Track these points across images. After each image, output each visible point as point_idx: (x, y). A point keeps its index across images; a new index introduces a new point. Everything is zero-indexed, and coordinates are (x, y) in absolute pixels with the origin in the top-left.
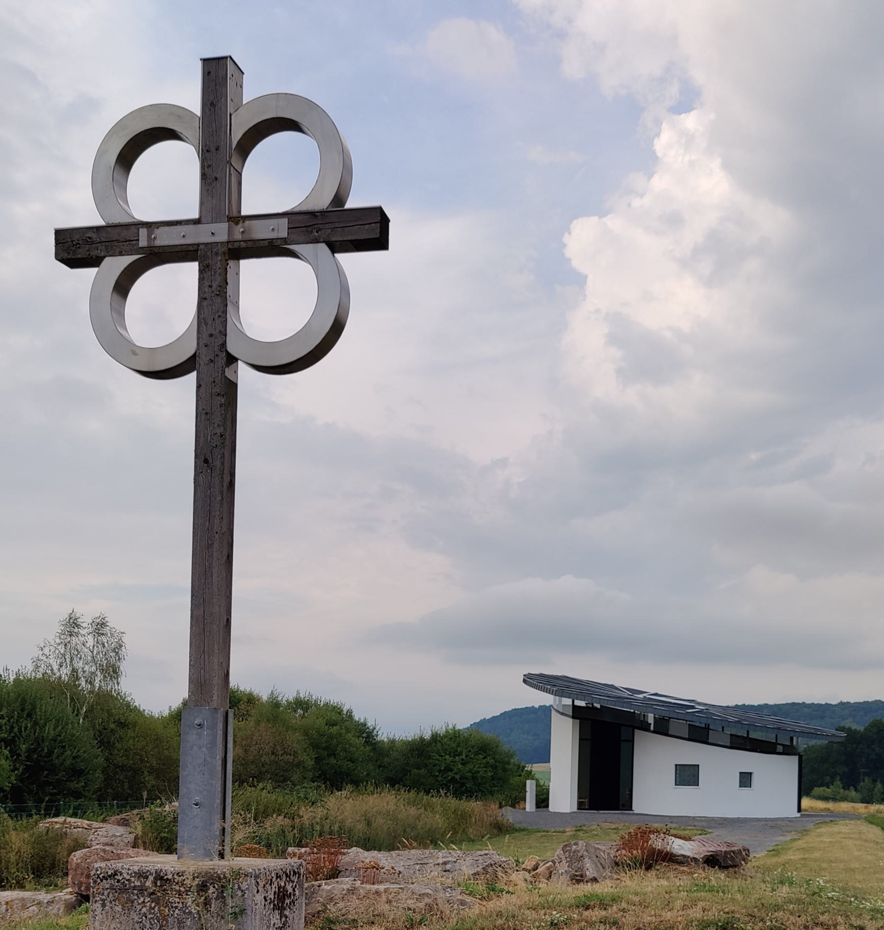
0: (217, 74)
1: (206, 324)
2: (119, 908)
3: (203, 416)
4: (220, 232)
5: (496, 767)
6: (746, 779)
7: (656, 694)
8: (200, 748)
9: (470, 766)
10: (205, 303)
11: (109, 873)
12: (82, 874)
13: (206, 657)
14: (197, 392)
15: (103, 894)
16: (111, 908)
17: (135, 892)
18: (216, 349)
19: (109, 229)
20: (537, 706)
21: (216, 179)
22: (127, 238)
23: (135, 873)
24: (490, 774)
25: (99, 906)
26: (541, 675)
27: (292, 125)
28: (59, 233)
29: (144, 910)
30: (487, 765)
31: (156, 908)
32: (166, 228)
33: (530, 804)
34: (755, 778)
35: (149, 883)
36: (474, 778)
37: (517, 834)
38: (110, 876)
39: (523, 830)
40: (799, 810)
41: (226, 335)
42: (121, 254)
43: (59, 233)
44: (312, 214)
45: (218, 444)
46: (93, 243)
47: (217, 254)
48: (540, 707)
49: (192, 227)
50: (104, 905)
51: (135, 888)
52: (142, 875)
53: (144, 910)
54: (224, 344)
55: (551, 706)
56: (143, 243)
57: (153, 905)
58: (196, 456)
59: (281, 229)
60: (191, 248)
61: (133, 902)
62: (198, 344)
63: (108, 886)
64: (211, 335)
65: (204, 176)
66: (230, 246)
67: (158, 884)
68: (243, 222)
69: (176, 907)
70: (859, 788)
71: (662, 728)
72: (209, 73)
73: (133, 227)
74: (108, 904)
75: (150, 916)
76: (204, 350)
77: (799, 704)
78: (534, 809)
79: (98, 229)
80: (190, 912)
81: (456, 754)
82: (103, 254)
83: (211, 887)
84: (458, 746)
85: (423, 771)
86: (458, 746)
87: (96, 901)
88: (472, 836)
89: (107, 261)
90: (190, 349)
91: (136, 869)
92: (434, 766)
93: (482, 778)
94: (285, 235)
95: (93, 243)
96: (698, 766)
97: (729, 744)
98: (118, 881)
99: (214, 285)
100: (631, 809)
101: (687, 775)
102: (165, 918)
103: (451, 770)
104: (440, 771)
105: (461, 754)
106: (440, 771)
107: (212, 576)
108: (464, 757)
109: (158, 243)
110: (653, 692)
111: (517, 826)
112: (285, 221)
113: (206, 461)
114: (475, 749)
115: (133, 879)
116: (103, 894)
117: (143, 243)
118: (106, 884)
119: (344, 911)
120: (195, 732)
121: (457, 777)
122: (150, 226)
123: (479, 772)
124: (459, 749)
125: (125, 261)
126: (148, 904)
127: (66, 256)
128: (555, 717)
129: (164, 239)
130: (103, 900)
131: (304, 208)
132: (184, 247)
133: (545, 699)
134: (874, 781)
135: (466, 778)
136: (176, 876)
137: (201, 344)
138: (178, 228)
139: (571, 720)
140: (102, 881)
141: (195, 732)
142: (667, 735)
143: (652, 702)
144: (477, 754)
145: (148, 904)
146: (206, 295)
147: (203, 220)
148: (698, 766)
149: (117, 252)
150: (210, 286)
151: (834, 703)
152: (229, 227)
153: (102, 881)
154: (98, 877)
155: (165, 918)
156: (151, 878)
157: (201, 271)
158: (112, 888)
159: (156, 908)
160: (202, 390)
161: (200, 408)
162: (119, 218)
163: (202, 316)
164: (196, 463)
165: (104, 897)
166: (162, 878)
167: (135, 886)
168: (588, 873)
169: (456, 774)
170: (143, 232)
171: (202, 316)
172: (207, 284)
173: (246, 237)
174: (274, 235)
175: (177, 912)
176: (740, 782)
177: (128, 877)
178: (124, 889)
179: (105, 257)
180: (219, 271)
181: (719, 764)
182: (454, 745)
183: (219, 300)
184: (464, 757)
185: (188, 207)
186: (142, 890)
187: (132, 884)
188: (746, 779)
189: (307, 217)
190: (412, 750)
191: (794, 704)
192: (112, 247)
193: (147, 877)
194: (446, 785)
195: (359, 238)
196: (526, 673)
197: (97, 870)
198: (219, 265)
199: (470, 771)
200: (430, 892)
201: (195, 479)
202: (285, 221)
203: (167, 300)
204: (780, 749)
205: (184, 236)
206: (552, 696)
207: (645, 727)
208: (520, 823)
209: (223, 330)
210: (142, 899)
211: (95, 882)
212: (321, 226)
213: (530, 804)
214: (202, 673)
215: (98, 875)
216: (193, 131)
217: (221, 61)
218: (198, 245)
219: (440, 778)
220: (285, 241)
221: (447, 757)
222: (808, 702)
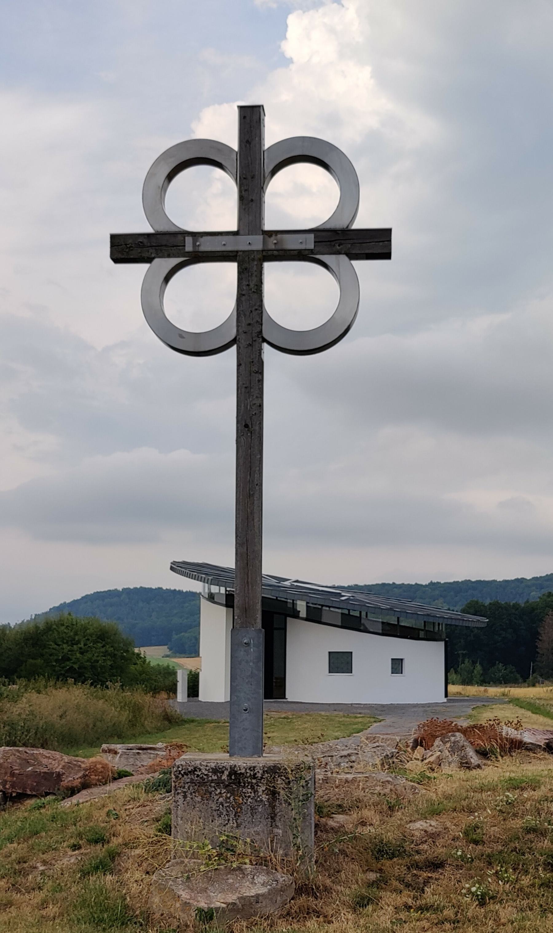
0: (251, 119)
1: (245, 315)
2: (199, 799)
3: (243, 390)
4: (256, 243)
5: (115, 655)
6: (397, 666)
7: (297, 581)
8: (247, 662)
9: (89, 655)
10: (243, 298)
11: (190, 770)
12: (6, 773)
13: (250, 587)
14: (238, 370)
15: (184, 788)
16: (192, 798)
17: (213, 784)
18: (254, 335)
19: (158, 236)
20: (120, 589)
21: (252, 200)
22: (175, 244)
23: (212, 769)
24: (109, 663)
25: (181, 797)
26: (184, 563)
27: (325, 166)
28: (114, 237)
29: (221, 799)
30: (105, 654)
31: (232, 798)
32: (209, 238)
33: (182, 695)
34: (406, 664)
35: (224, 777)
36: (93, 667)
37: (187, 726)
38: (190, 772)
39: (193, 721)
40: (446, 696)
41: (262, 325)
42: (169, 256)
43: (114, 237)
44: (334, 231)
45: (257, 412)
46: (144, 246)
47: (253, 260)
48: (124, 590)
49: (231, 237)
50: (185, 797)
51: (212, 781)
52: (216, 771)
53: (221, 799)
54: (261, 332)
55: (200, 593)
56: (189, 248)
57: (229, 795)
58: (238, 422)
59: (309, 243)
60: (231, 254)
61: (211, 793)
62: (238, 331)
63: (189, 780)
64: (249, 324)
65: (241, 198)
66: (264, 253)
67: (233, 777)
68: (276, 235)
69: (249, 797)
70: (459, 669)
71: (315, 616)
72: (245, 117)
73: (179, 236)
74: (189, 796)
75: (226, 805)
76: (243, 336)
77: (389, 584)
78: (186, 700)
79: (148, 235)
80: (261, 801)
81: (73, 642)
82: (153, 256)
83: (279, 779)
84: (76, 634)
85: (39, 661)
86: (76, 634)
87: (178, 793)
88: (149, 729)
89: (157, 261)
90: (232, 333)
91: (213, 765)
92: (51, 655)
93: (102, 667)
94: (312, 247)
95: (144, 246)
96: (351, 653)
97: (381, 632)
98: (198, 776)
99: (252, 286)
100: (284, 697)
101: (340, 663)
102: (239, 806)
103: (69, 659)
104: (56, 661)
105: (78, 642)
106: (56, 661)
107: (253, 520)
108: (82, 645)
109: (202, 249)
110: (294, 579)
111: (185, 717)
112: (312, 236)
113: (246, 426)
114: (94, 638)
115: (210, 774)
116: (184, 788)
117: (189, 248)
118: (187, 779)
119: (326, 798)
120: (242, 649)
121: (76, 666)
122: (195, 235)
123: (98, 661)
124: (77, 638)
125: (174, 261)
126: (224, 795)
127: (120, 256)
128: (205, 606)
129: (206, 245)
130: (185, 792)
131: (328, 226)
132: (225, 254)
133: (195, 586)
134: (474, 663)
135: (85, 668)
136: (248, 771)
137: (240, 331)
138: (219, 238)
139: (224, 609)
140: (183, 776)
141: (242, 649)
142: (320, 622)
143: (302, 590)
144: (95, 642)
145: (224, 795)
146: (244, 293)
147: (241, 232)
148: (351, 653)
149: (166, 255)
150: (248, 285)
151: (424, 584)
152: (264, 239)
153: (183, 776)
154: (180, 773)
155: (239, 806)
156: (226, 773)
157: (240, 273)
158: (192, 781)
159: (232, 798)
160: (243, 367)
161: (241, 383)
162: (163, 228)
163: (241, 308)
164: (237, 428)
165: (185, 790)
166: (235, 773)
167: (212, 780)
168: (472, 760)
169: (74, 663)
170: (189, 240)
171: (241, 308)
172: (245, 283)
173: (279, 247)
174: (302, 247)
175: (250, 800)
176: (392, 668)
177: (206, 773)
178: (203, 782)
179: (154, 258)
180: (255, 273)
181: (372, 651)
182: (72, 634)
183: (255, 296)
184: (82, 645)
185: (230, 223)
186: (219, 782)
187: (210, 778)
188: (397, 666)
189: (329, 233)
190: (26, 640)
191: (384, 585)
192: (161, 250)
193: (223, 772)
194: (64, 675)
195: (375, 252)
196: (172, 561)
197: (179, 767)
198: (255, 268)
199: (88, 661)
200: (391, 780)
201: (237, 440)
202: (312, 236)
203: (206, 295)
204: (422, 634)
205: (224, 245)
206: (201, 584)
207: (295, 615)
208: (185, 714)
209: (260, 320)
210: (219, 791)
211: (177, 777)
212: (342, 242)
213: (182, 695)
214: (247, 599)
215: (180, 771)
216: (232, 162)
217: (255, 109)
218: (237, 252)
219: (57, 668)
220: (312, 251)
221: (65, 646)
222: (398, 582)
